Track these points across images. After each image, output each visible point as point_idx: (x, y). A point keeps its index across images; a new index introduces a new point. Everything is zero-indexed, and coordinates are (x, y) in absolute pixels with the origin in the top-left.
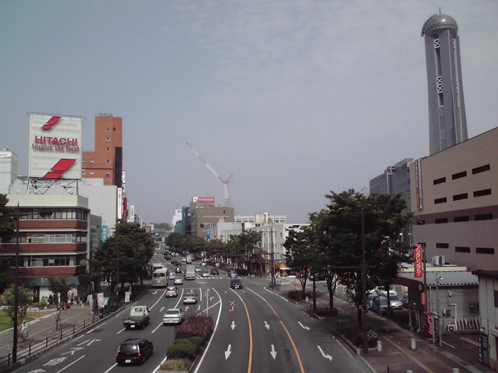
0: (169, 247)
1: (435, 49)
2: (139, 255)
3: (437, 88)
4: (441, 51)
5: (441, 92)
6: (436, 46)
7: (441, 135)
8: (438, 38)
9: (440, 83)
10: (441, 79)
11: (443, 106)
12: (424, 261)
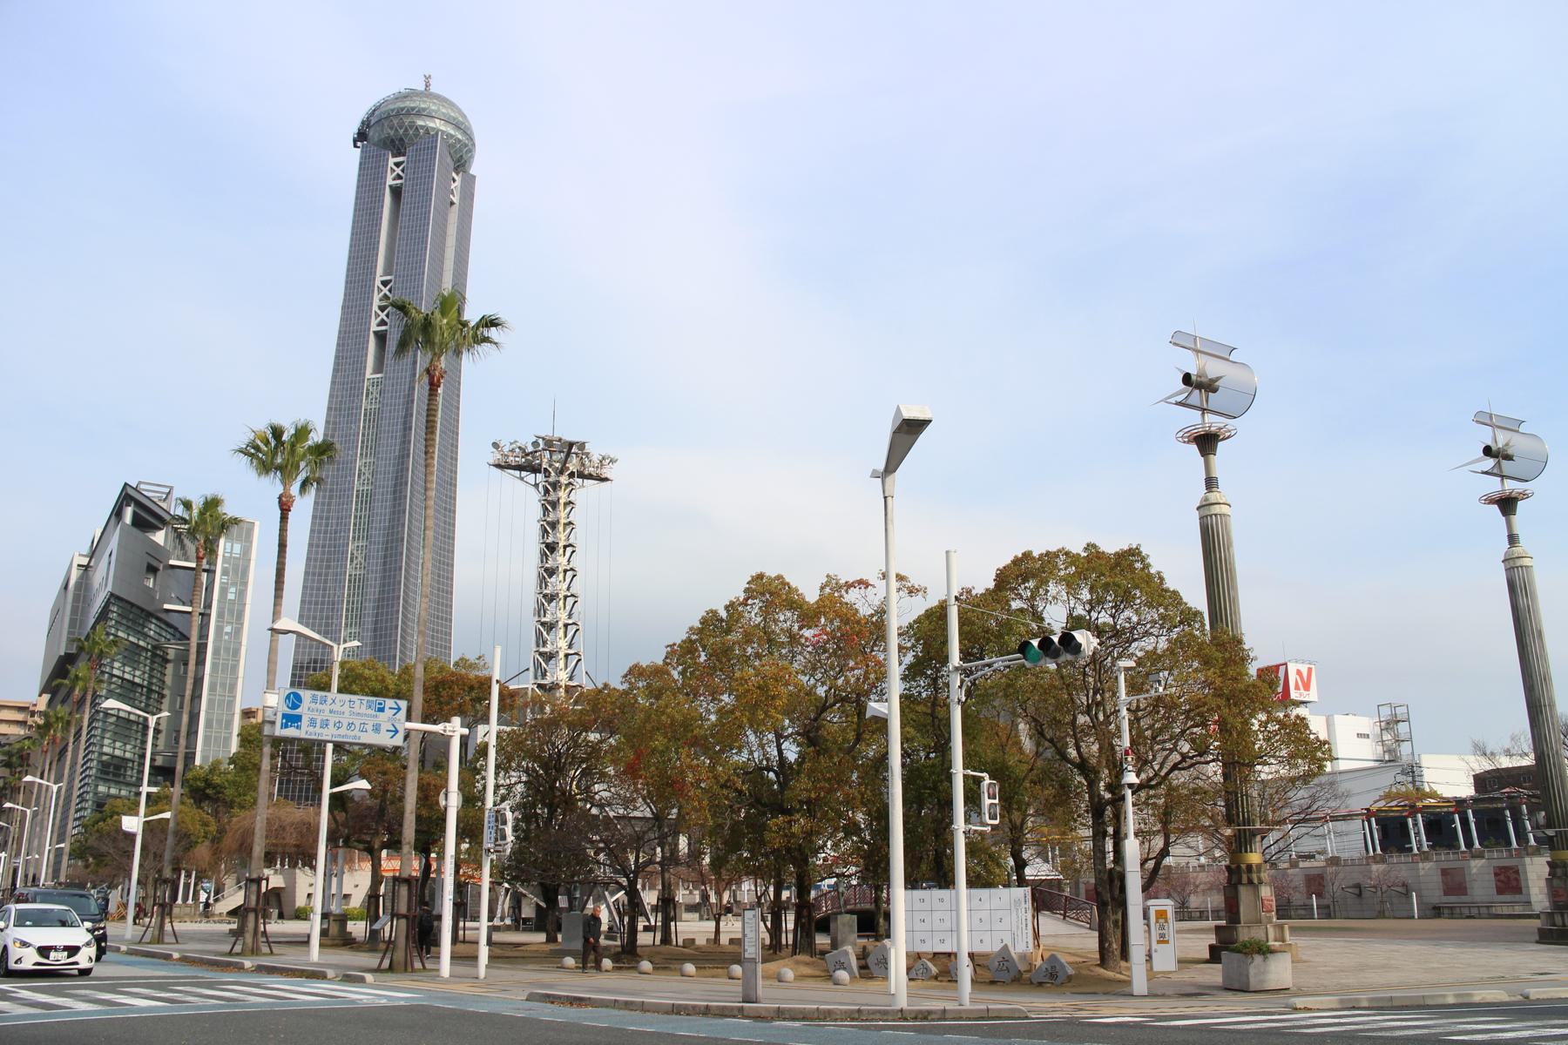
0: (674, 817)
1: (388, 190)
2: (520, 788)
3: (376, 288)
4: (405, 196)
5: (383, 328)
6: (379, 325)
7: (352, 561)
8: (404, 155)
9: (386, 297)
10: (386, 312)
11: (379, 375)
12: (60, 696)
